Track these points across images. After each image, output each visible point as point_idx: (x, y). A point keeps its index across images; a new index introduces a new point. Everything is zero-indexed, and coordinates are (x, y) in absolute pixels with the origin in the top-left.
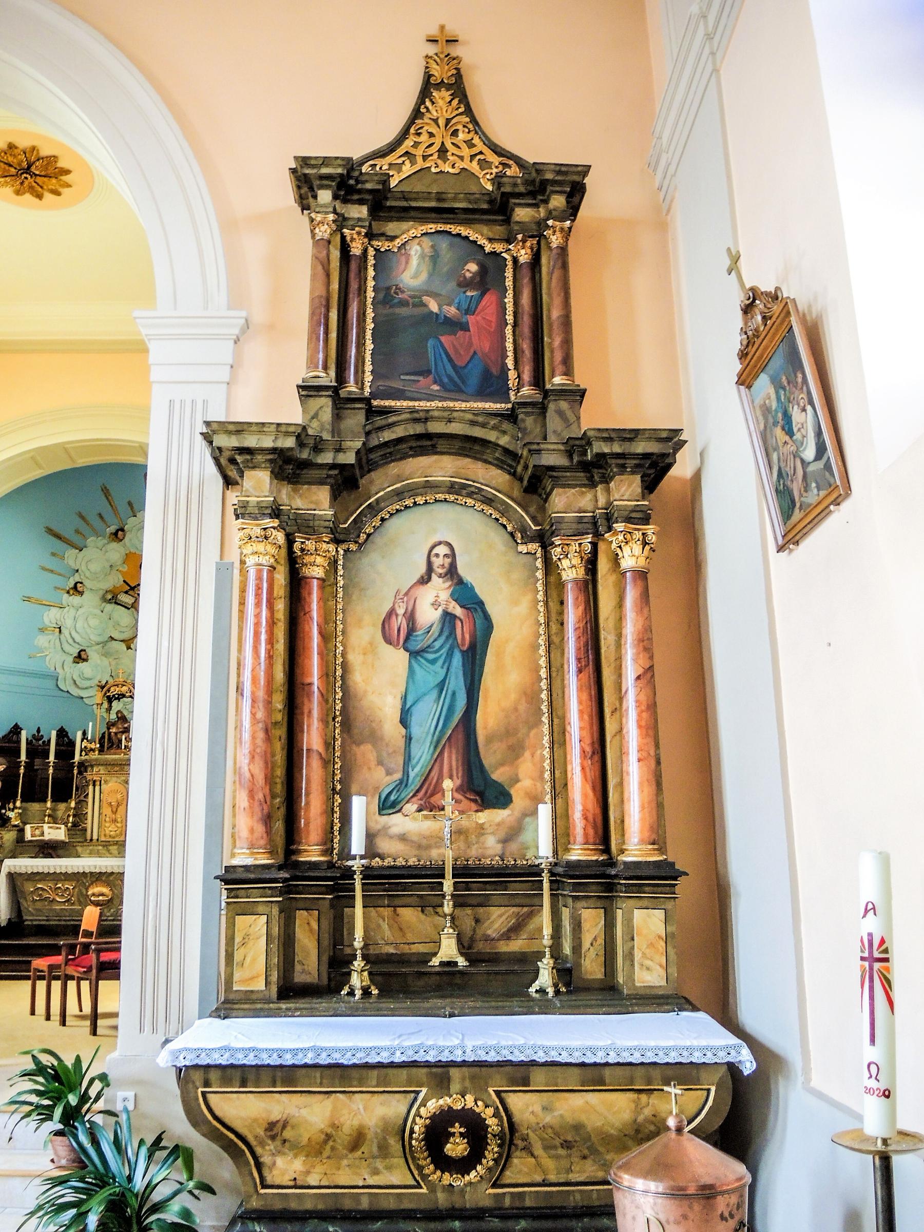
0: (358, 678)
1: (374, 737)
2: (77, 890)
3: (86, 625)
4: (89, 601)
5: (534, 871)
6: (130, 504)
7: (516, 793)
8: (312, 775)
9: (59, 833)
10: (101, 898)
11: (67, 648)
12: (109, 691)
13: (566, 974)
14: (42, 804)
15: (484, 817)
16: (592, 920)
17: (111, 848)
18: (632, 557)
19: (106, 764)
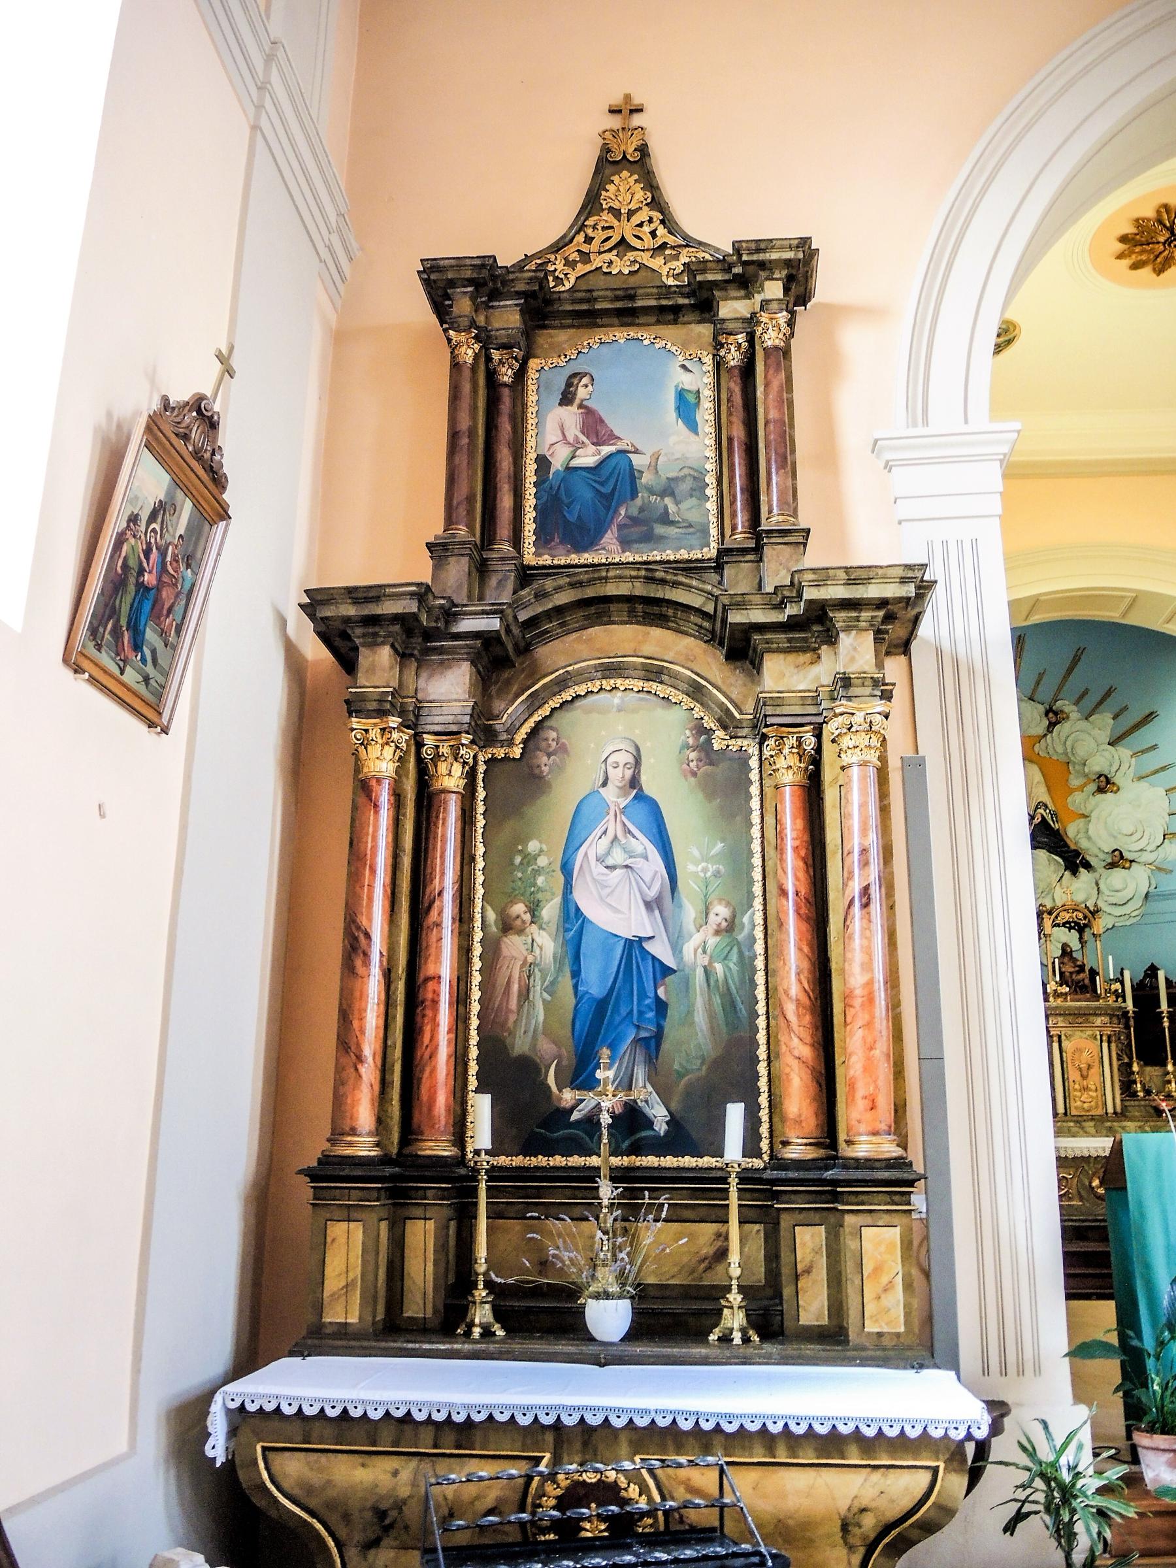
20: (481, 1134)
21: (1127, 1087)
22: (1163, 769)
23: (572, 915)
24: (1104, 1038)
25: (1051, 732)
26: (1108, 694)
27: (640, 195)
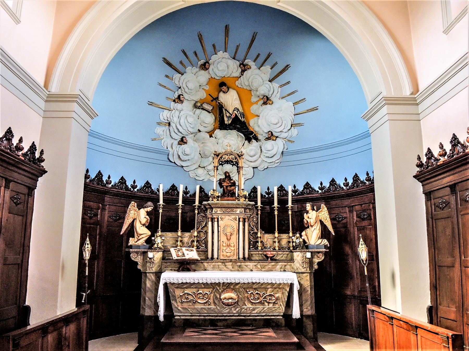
2: (212, 295)
3: (186, 122)
4: (187, 106)
6: (214, 46)
9: (192, 254)
10: (230, 301)
12: (221, 158)
14: (173, 233)
17: (227, 264)
21: (253, 245)
22: (293, 93)
24: (241, 220)
25: (243, 75)
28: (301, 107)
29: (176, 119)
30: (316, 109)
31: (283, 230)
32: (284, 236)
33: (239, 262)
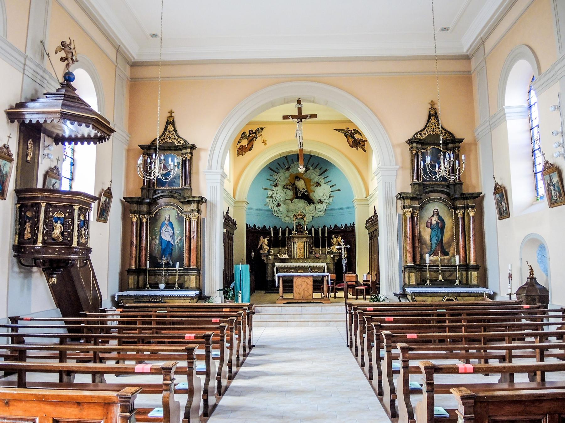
0: (422, 233)
1: (426, 244)
4: (280, 188)
5: (456, 266)
7: (450, 253)
8: (418, 251)
9: (286, 256)
11: (274, 202)
13: (460, 282)
15: (445, 257)
16: (464, 274)
18: (472, 214)
19: (297, 237)
20: (148, 266)
21: (310, 252)
23: (161, 238)
26: (318, 164)
27: (173, 129)
28: (334, 188)
29: (275, 195)
30: (340, 190)
31: (323, 246)
32: (324, 249)
33: (304, 260)
